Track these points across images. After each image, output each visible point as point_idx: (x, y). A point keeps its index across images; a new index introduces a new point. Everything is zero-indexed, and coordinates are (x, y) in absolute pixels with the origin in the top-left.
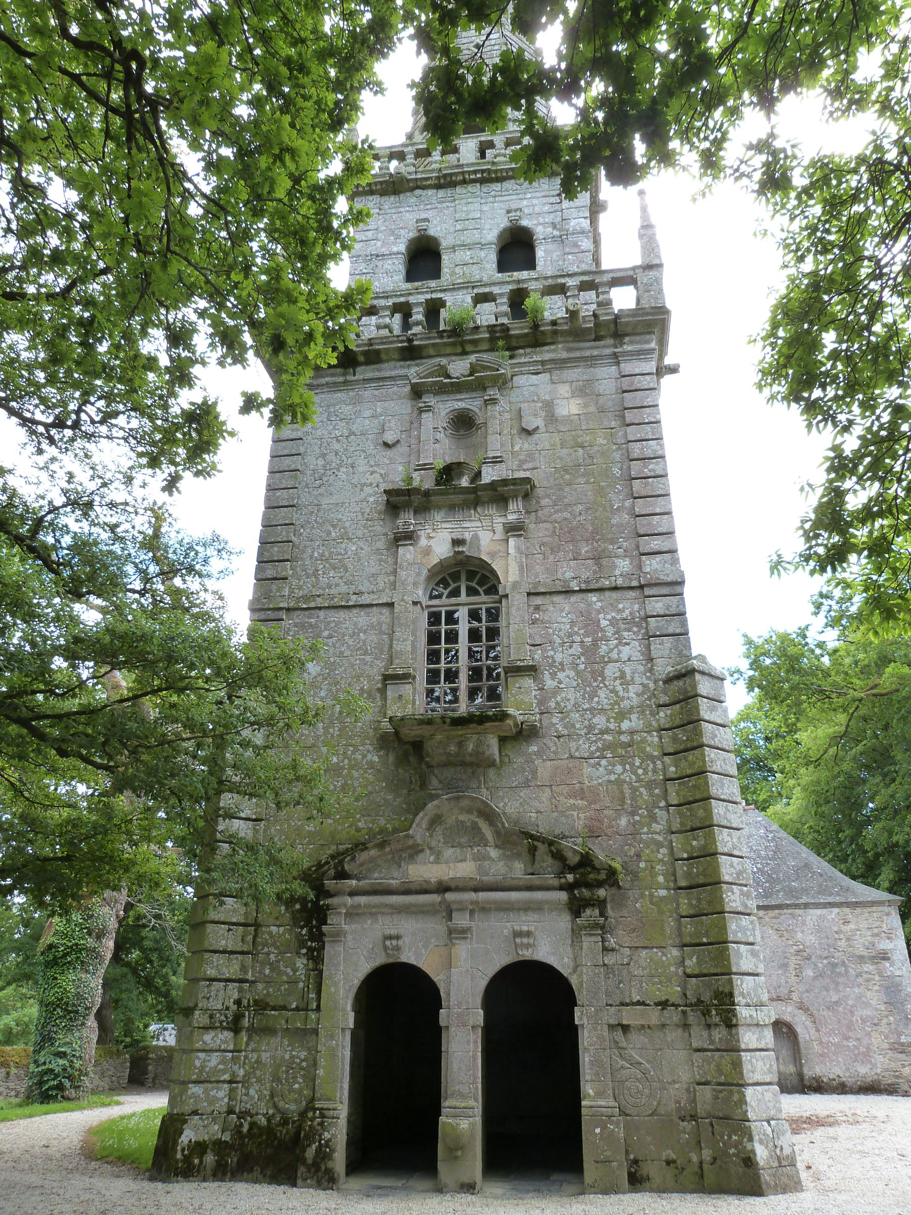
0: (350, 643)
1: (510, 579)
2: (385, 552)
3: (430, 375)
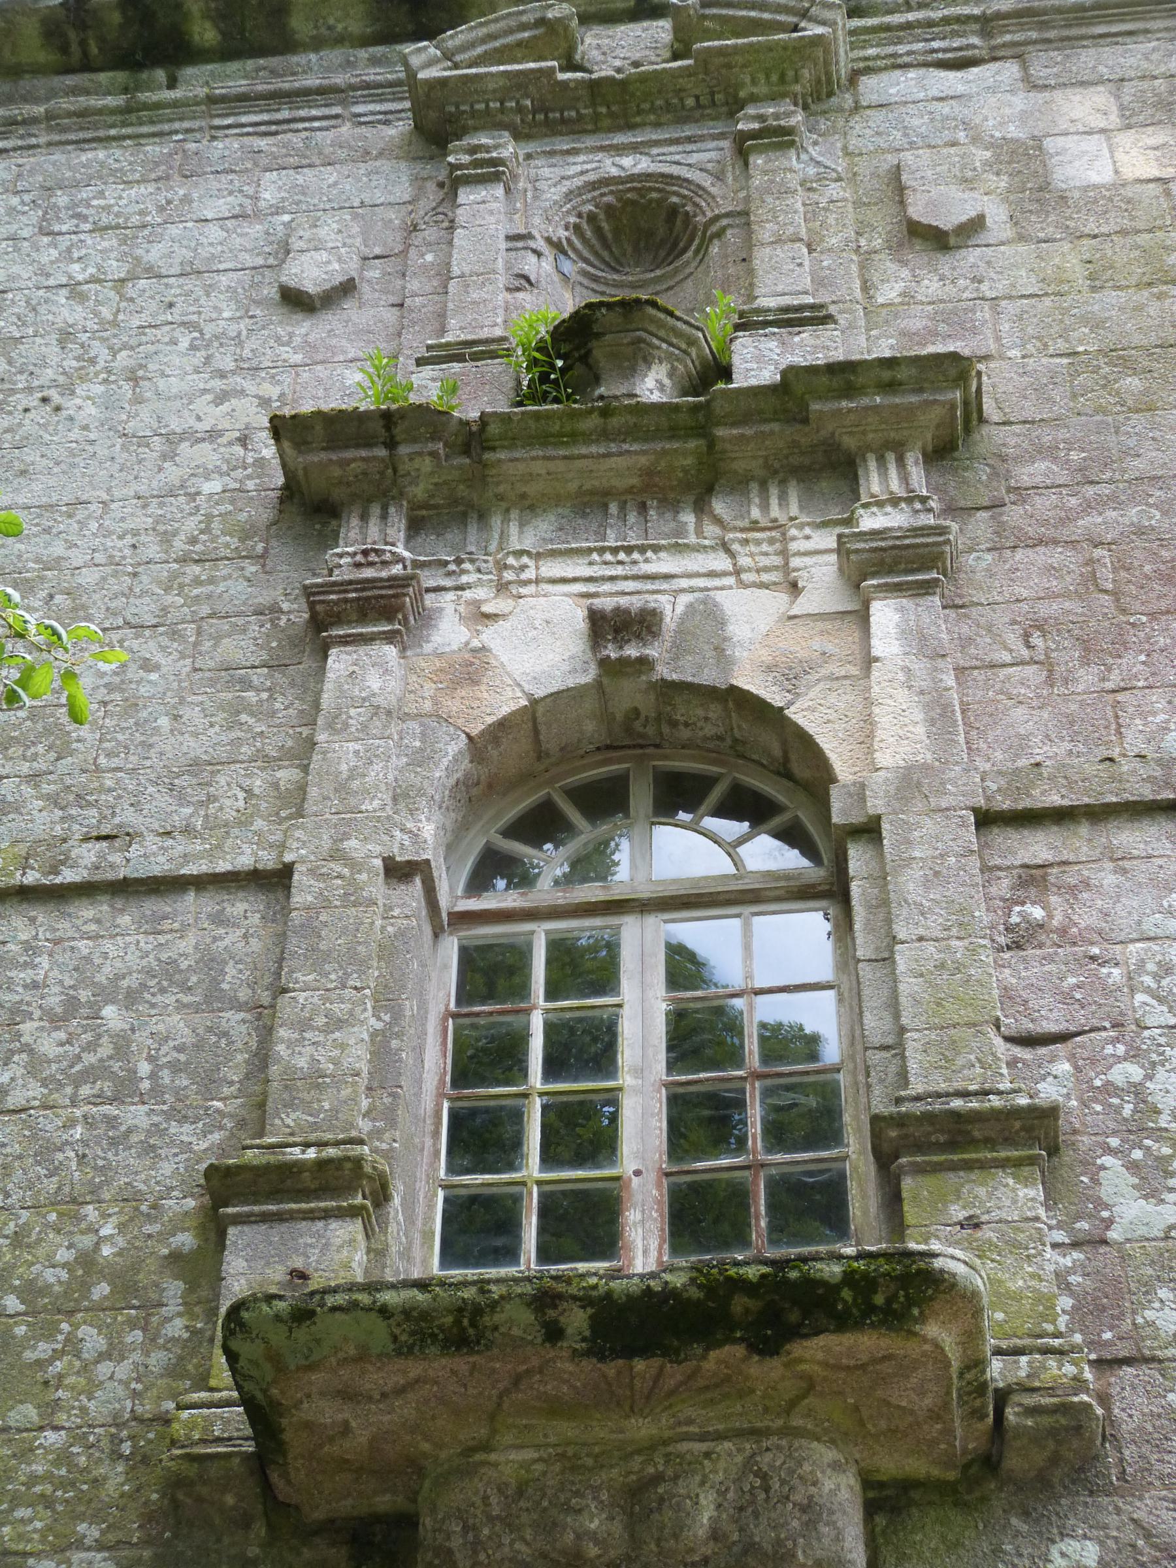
0: (48, 1046)
1: (884, 758)
2: (258, 677)
3: (498, 56)
